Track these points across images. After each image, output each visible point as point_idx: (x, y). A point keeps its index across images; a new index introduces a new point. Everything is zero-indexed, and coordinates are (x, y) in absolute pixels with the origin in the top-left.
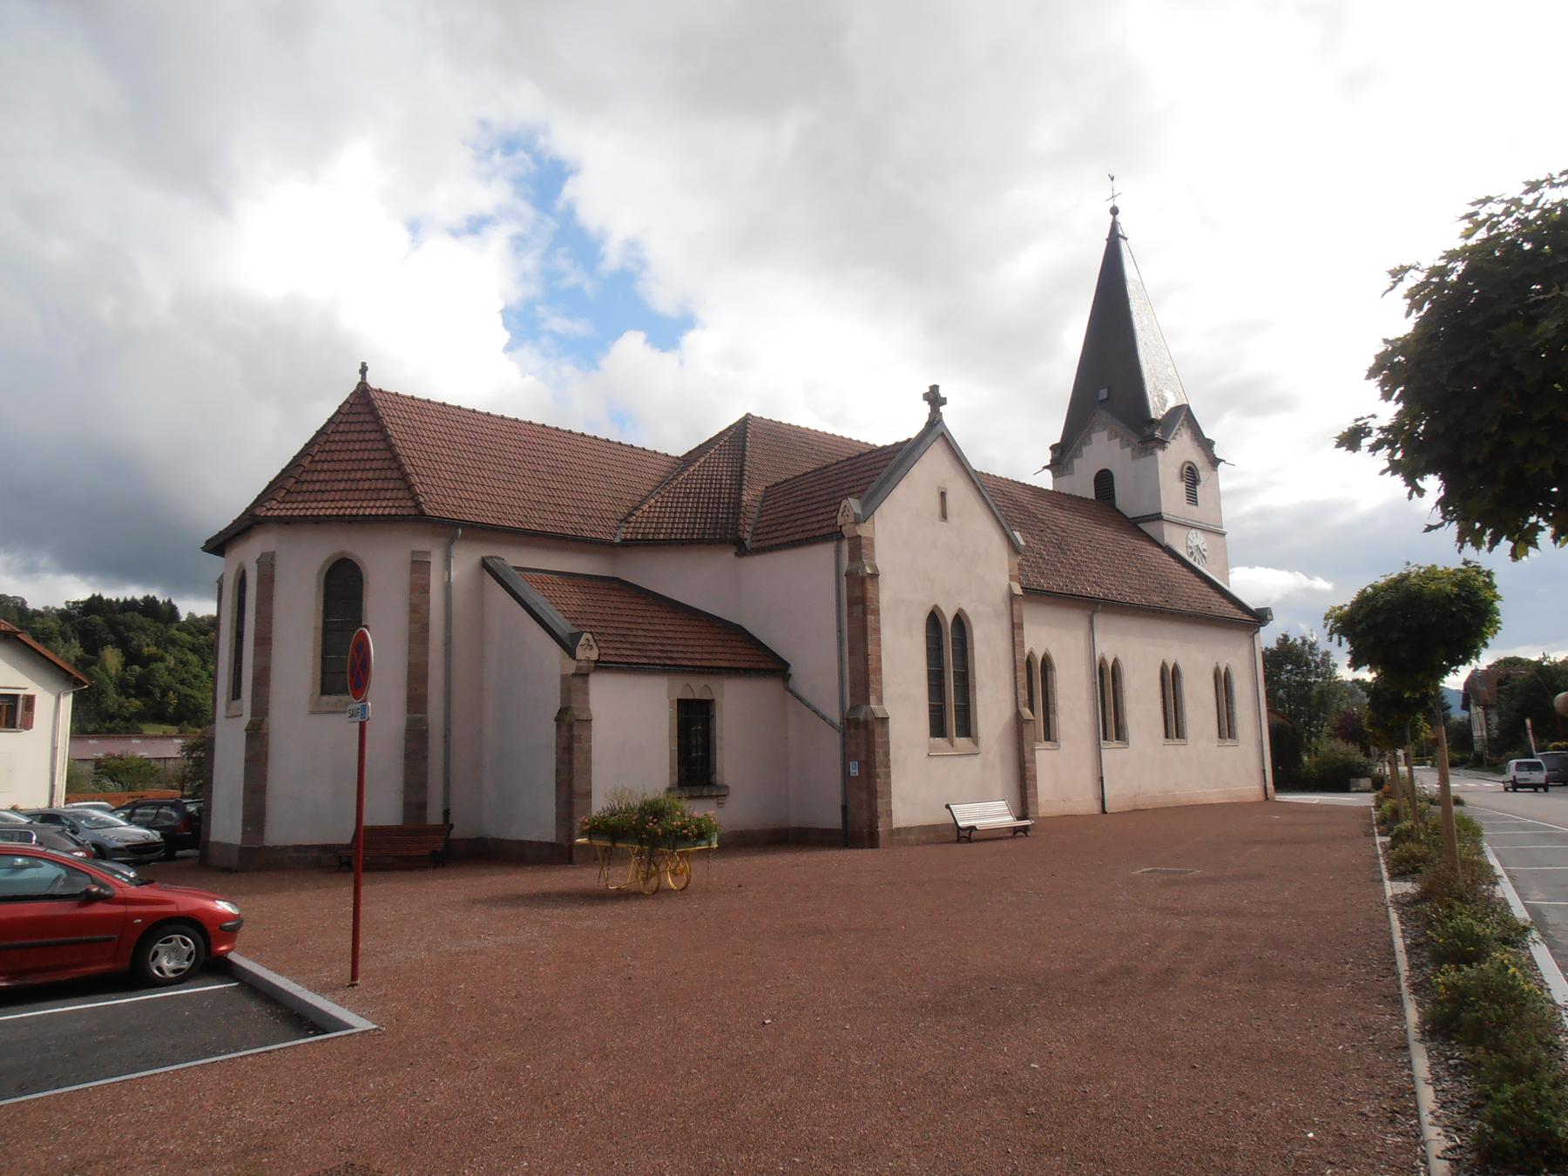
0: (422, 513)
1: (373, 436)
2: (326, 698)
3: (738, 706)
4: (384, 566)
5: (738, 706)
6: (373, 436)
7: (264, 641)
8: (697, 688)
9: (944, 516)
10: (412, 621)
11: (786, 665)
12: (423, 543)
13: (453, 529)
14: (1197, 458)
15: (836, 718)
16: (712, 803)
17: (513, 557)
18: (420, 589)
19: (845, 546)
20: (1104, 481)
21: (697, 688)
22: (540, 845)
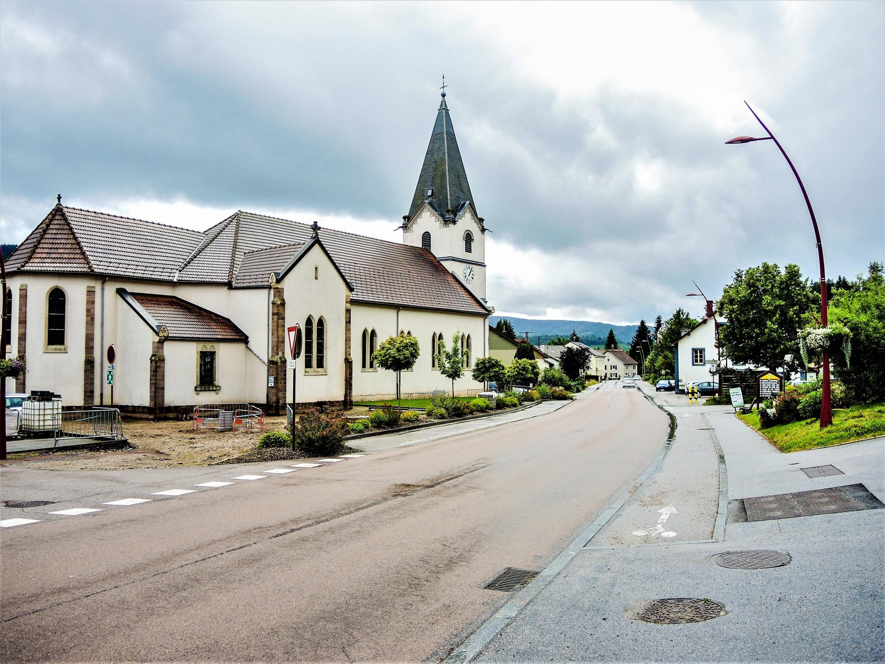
0: (93, 271)
1: (78, 256)
2: (50, 347)
3: (227, 356)
4: (76, 293)
5: (227, 356)
6: (78, 256)
7: (23, 322)
8: (208, 347)
9: (316, 278)
10: (87, 316)
11: (247, 337)
12: (92, 283)
13: (104, 278)
14: (475, 229)
15: (266, 361)
16: (213, 393)
17: (130, 288)
18: (91, 303)
19: (272, 291)
20: (426, 237)
21: (208, 347)
22: (144, 407)
